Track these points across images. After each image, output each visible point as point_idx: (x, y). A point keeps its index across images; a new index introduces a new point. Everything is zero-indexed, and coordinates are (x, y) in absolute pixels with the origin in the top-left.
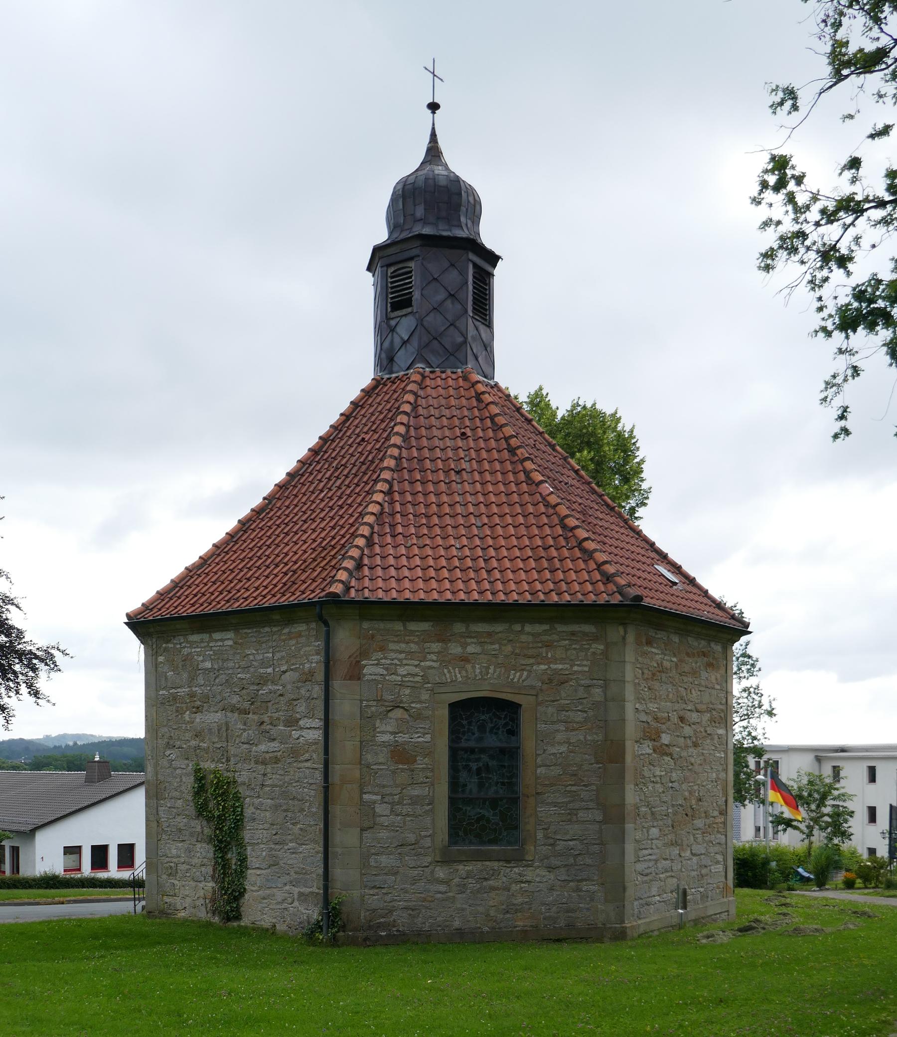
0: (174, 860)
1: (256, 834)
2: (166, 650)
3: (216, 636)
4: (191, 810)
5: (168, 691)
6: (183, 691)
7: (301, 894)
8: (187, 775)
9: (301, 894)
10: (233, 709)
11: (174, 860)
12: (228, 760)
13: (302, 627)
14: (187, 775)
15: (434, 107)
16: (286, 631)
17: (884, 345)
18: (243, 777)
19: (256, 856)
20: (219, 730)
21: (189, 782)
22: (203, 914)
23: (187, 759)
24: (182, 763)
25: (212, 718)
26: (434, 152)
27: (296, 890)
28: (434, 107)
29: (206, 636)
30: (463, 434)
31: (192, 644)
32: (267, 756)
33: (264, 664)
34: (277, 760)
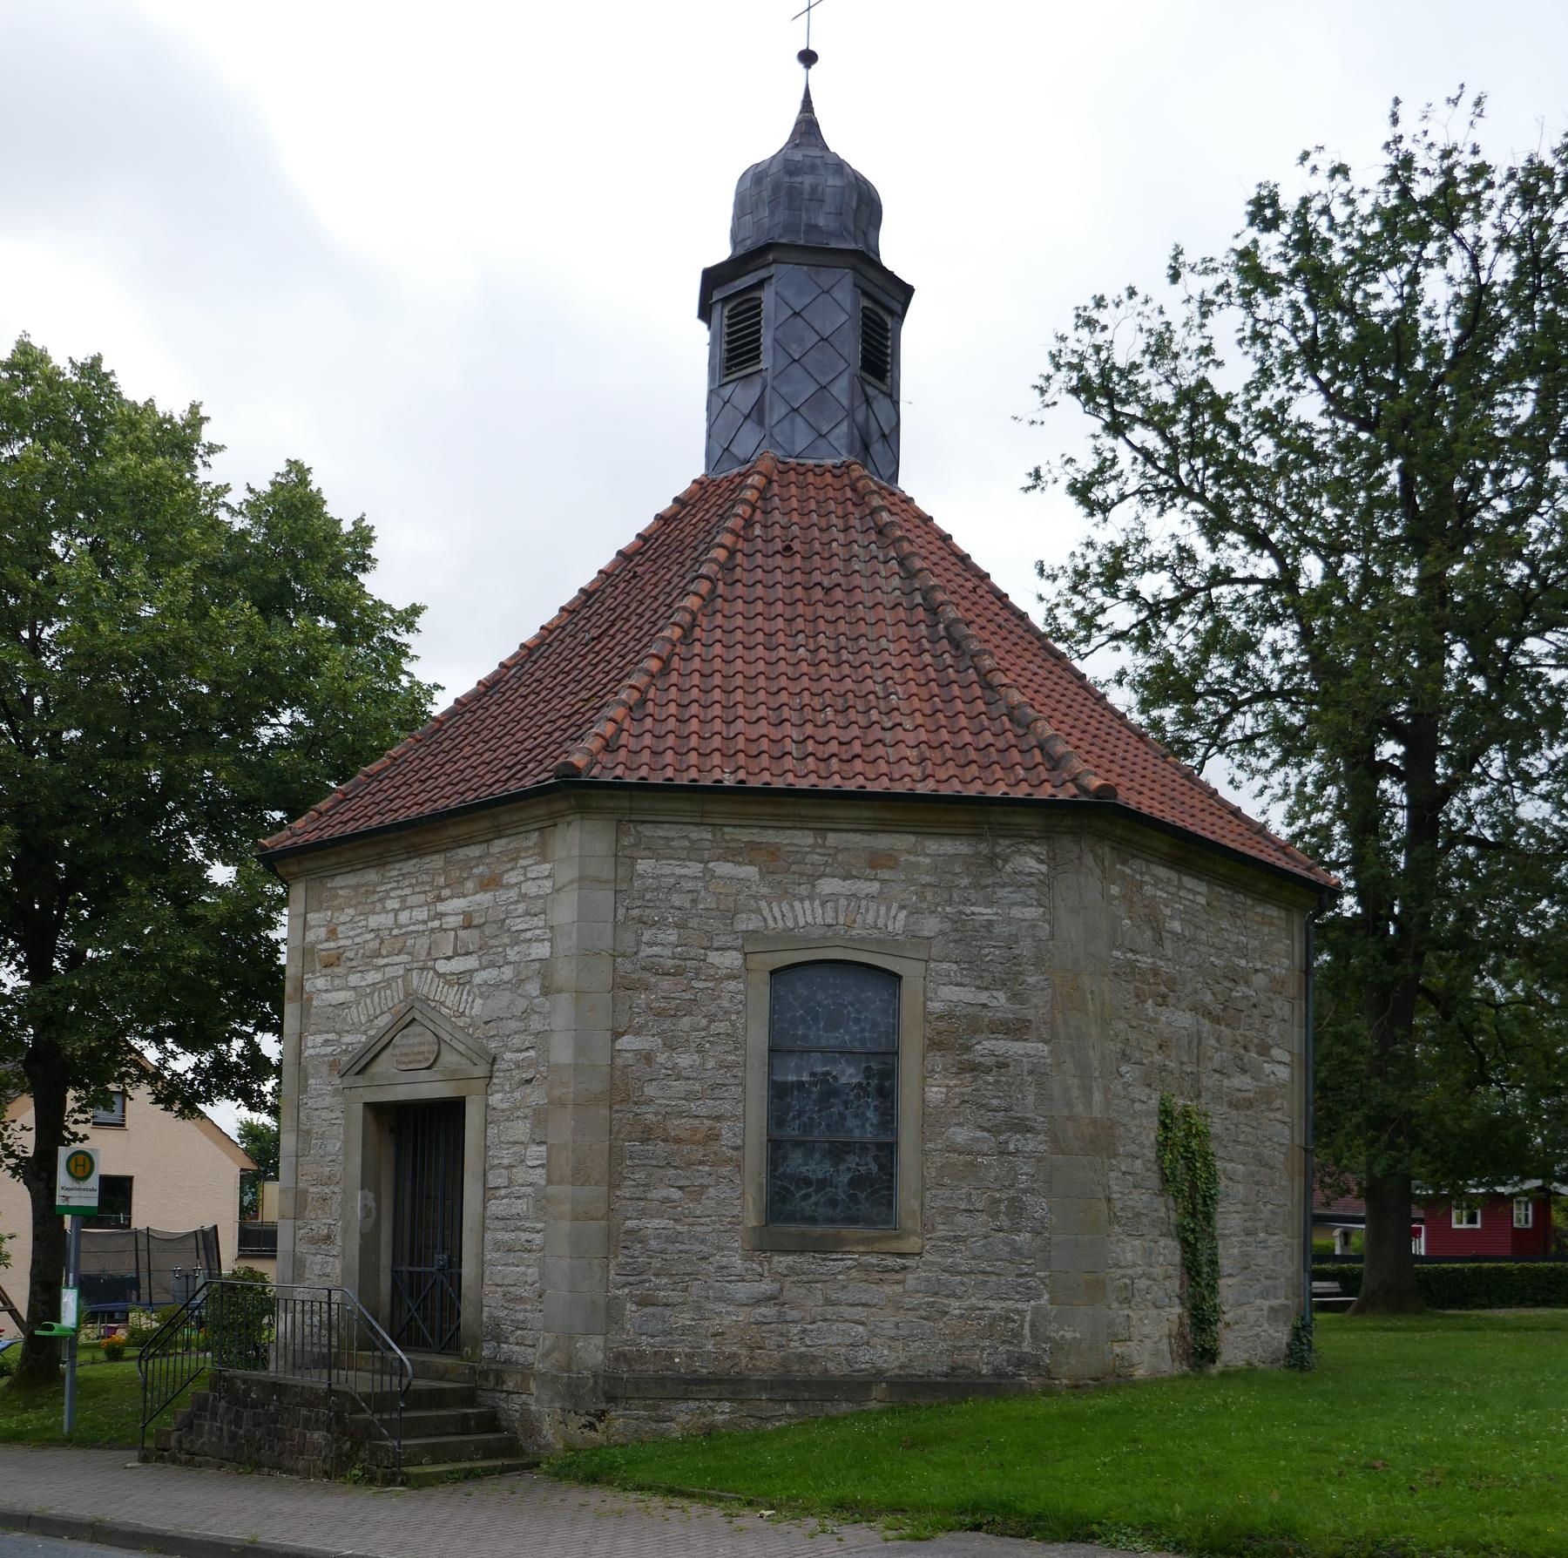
0: (1129, 1272)
1: (1228, 1219)
2: (1124, 876)
3: (1189, 882)
4: (1154, 1180)
5: (1124, 953)
6: (1145, 961)
7: (1271, 1308)
8: (1148, 1114)
9: (1271, 1308)
10: (1208, 1014)
11: (1129, 1272)
12: (1198, 1096)
13: (1273, 912)
14: (1148, 1114)
15: (808, 58)
16: (1259, 909)
17: (196, 420)
18: (1216, 1127)
19: (1228, 1253)
20: (1190, 1042)
21: (1150, 1132)
22: (1168, 1367)
23: (1149, 1086)
24: (1139, 1092)
25: (1181, 1020)
26: (807, 127)
27: (1266, 1304)
28: (808, 58)
29: (1173, 875)
30: (788, 548)
31: (1157, 881)
32: (1240, 1095)
33: (1242, 951)
34: (1250, 1104)
